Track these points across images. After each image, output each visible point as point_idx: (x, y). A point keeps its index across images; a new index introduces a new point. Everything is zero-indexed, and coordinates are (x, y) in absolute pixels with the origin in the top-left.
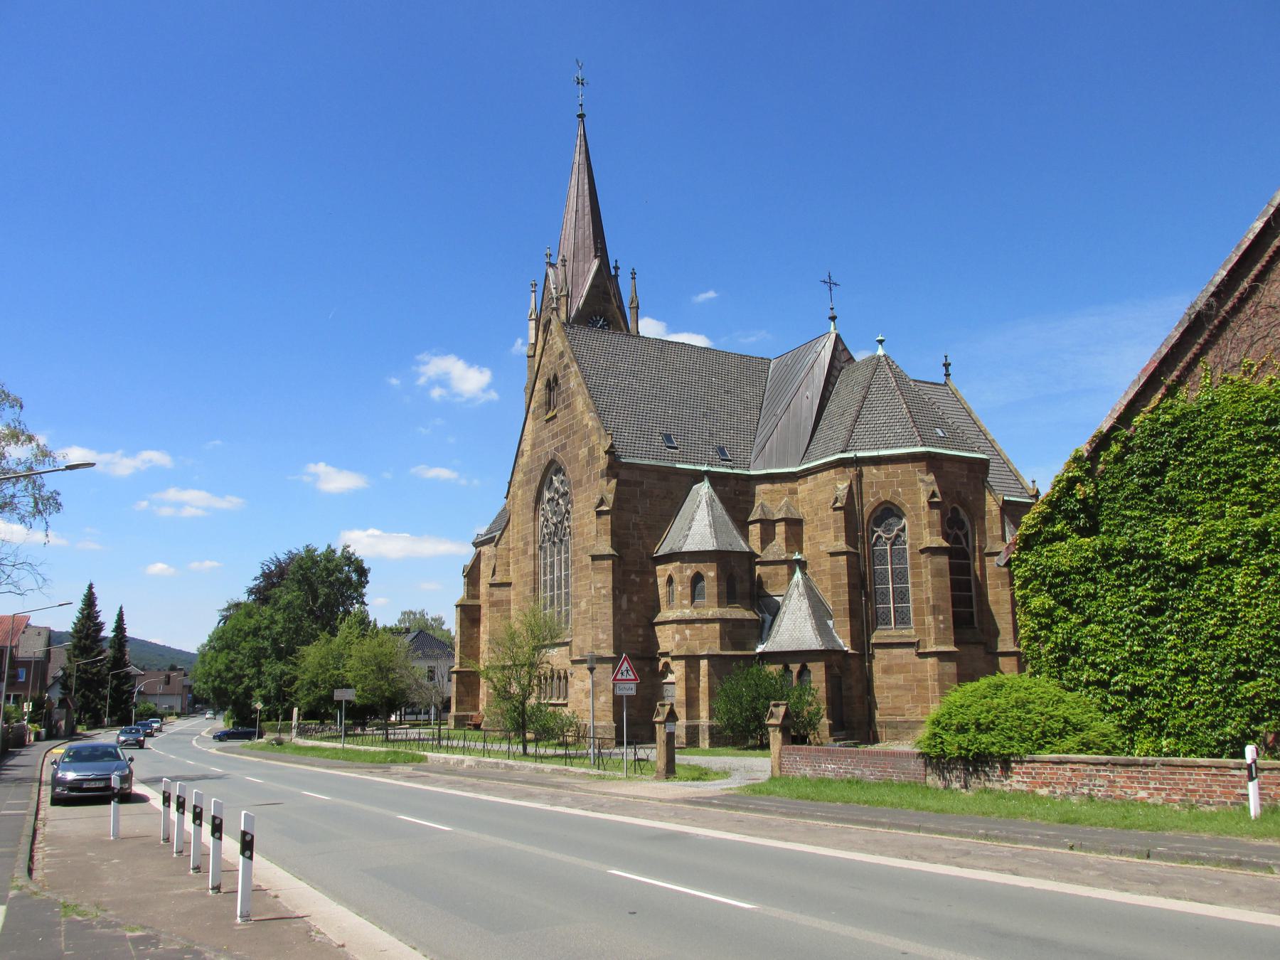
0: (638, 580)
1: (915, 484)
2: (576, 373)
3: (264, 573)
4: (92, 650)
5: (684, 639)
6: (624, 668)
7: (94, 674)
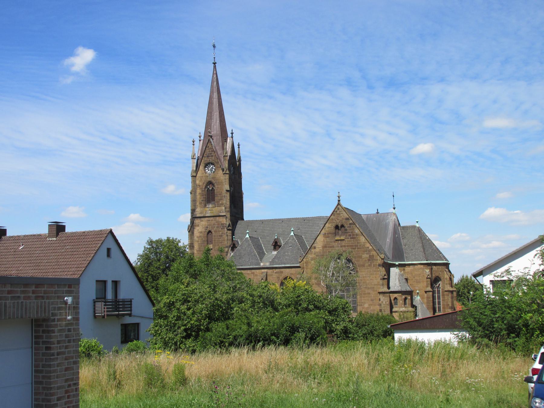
1: (443, 271)
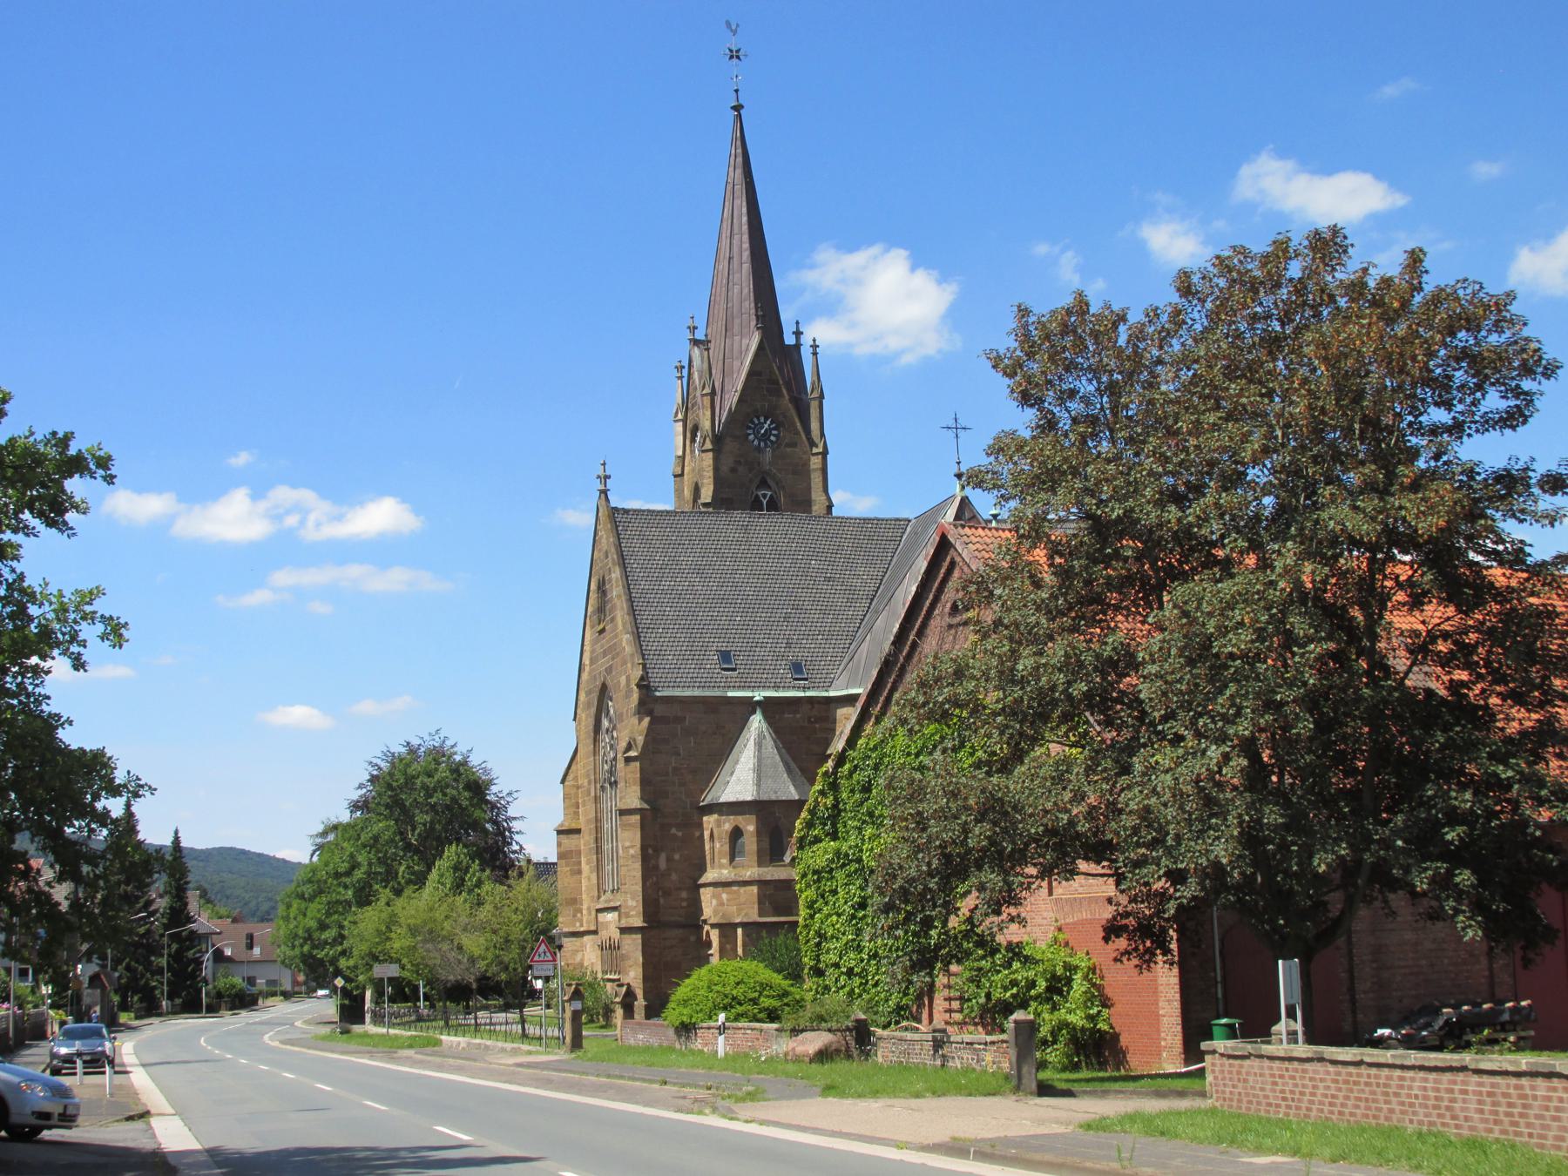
0: (680, 834)
2: (617, 581)
3: (372, 776)
4: (137, 898)
5: (722, 904)
6: (541, 950)
7: (143, 936)
